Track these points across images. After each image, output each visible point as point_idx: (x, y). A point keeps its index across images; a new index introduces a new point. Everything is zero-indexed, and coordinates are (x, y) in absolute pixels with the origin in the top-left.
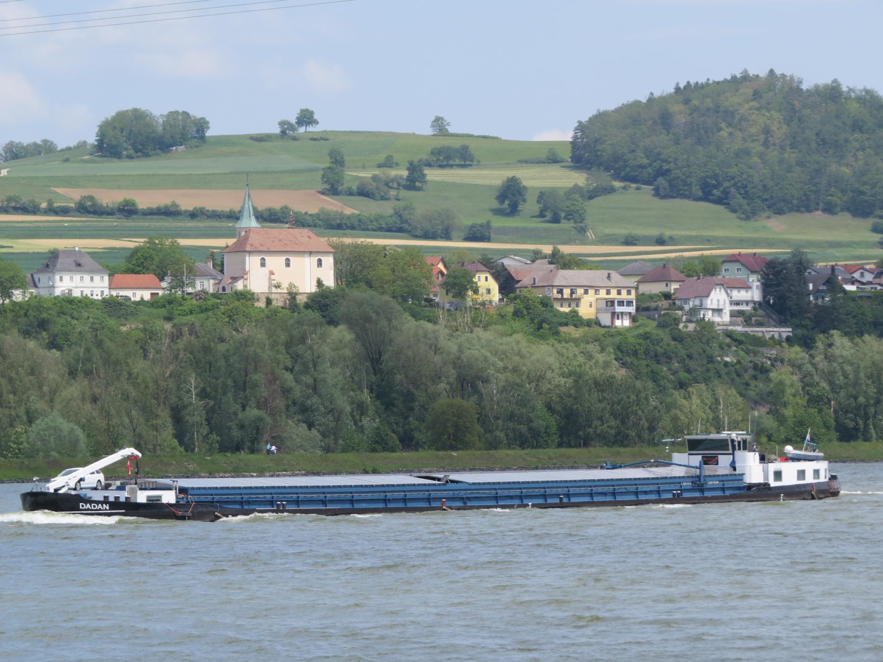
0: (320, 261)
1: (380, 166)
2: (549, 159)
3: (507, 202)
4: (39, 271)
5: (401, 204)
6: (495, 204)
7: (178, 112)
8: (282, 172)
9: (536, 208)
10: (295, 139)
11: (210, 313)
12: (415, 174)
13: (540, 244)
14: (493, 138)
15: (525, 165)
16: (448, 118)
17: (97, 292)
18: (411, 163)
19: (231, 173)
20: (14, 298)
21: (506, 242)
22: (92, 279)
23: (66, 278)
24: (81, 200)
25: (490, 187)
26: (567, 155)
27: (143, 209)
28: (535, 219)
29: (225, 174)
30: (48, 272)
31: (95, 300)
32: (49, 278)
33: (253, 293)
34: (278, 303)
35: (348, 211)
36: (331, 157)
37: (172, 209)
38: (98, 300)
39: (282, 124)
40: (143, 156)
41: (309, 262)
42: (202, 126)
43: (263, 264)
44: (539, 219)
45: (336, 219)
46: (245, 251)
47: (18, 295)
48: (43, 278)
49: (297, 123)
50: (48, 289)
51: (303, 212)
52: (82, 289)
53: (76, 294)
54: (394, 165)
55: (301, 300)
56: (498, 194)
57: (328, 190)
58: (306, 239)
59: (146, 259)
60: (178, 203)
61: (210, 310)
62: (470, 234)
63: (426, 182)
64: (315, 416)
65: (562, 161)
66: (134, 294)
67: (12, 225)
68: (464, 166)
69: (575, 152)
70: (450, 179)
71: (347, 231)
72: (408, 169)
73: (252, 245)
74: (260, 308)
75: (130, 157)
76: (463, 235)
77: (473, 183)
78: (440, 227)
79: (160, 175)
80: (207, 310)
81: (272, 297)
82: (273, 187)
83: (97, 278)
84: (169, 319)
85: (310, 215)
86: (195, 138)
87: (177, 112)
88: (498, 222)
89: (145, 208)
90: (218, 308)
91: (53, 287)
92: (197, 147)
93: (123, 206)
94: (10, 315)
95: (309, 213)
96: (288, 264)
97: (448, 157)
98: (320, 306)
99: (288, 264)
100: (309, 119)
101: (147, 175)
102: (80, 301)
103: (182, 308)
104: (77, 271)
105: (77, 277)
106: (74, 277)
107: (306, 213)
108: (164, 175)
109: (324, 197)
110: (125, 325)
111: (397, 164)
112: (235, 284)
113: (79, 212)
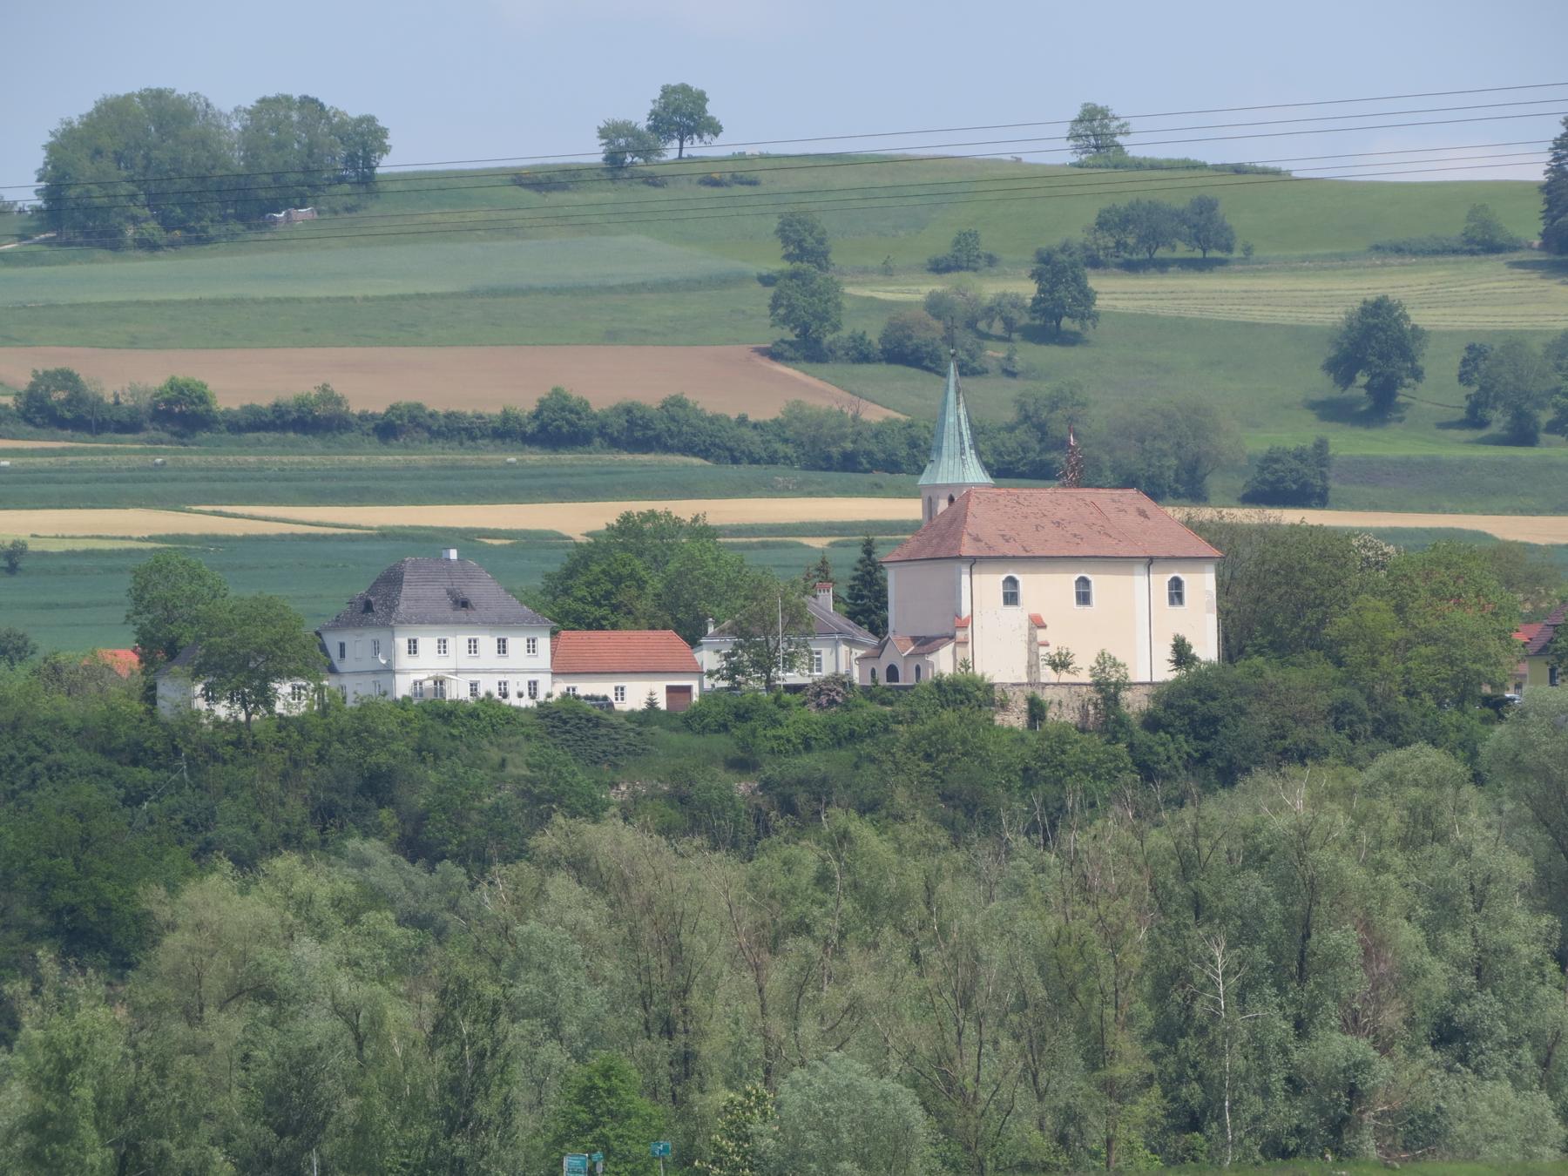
0: (1176, 585)
1: (939, 267)
2: (1471, 241)
3: (1362, 379)
4: (340, 623)
5: (1044, 388)
6: (1323, 386)
7: (288, 99)
8: (631, 289)
9: (1457, 398)
10: (652, 181)
11: (867, 747)
12: (1061, 292)
13: (1484, 513)
14: (1265, 172)
15: (1395, 260)
16: (1119, 106)
17: (517, 684)
18: (1045, 258)
19: (473, 294)
20: (279, 707)
21: (1375, 507)
22: (502, 647)
23: (427, 643)
24: (32, 385)
25: (1296, 333)
26: (1529, 227)
27: (228, 411)
28: (1453, 433)
29: (454, 295)
30: (370, 625)
31: (518, 709)
32: (376, 643)
33: (992, 686)
34: (1063, 714)
35: (874, 415)
36: (786, 240)
37: (320, 412)
38: (527, 710)
39: (609, 133)
40: (188, 242)
41: (1145, 587)
42: (364, 145)
43: (1011, 598)
44: (1468, 434)
45: (843, 437)
46: (959, 558)
47: (288, 698)
48: (357, 646)
49: (654, 129)
50: (372, 678)
51: (734, 416)
52: (474, 678)
53: (458, 690)
54: (982, 262)
55: (1135, 703)
56: (1333, 353)
57: (791, 344)
58: (1131, 519)
59: (618, 580)
60: (338, 389)
61: (861, 738)
62: (1264, 482)
63: (1095, 316)
64: (1482, 1052)
65: (1514, 248)
66: (620, 691)
67: (52, 475)
68: (1201, 265)
69: (1554, 219)
70: (1165, 308)
71: (879, 477)
72: (1037, 276)
73: (977, 539)
74: (1011, 730)
75: (148, 246)
76: (1240, 484)
77: (1242, 318)
78: (1173, 462)
79: (255, 301)
80: (852, 736)
81: (1047, 695)
82: (611, 336)
83: (517, 643)
84: (742, 765)
85: (755, 426)
86: (341, 180)
87: (283, 101)
88: (1347, 443)
89: (235, 407)
90: (886, 730)
91: (390, 671)
92: (348, 209)
93: (167, 402)
94: (276, 760)
95: (752, 418)
96: (1084, 598)
97: (1153, 237)
98: (1192, 721)
99: (1084, 598)
100: (690, 117)
101: (217, 303)
102: (473, 714)
103: (780, 732)
104: (458, 622)
105: (458, 642)
106: (451, 642)
107: (742, 420)
108: (267, 301)
109: (779, 368)
110: (614, 785)
111: (992, 260)
112: (931, 658)
113: (30, 421)
